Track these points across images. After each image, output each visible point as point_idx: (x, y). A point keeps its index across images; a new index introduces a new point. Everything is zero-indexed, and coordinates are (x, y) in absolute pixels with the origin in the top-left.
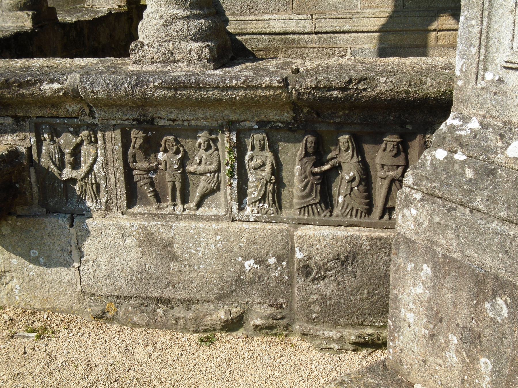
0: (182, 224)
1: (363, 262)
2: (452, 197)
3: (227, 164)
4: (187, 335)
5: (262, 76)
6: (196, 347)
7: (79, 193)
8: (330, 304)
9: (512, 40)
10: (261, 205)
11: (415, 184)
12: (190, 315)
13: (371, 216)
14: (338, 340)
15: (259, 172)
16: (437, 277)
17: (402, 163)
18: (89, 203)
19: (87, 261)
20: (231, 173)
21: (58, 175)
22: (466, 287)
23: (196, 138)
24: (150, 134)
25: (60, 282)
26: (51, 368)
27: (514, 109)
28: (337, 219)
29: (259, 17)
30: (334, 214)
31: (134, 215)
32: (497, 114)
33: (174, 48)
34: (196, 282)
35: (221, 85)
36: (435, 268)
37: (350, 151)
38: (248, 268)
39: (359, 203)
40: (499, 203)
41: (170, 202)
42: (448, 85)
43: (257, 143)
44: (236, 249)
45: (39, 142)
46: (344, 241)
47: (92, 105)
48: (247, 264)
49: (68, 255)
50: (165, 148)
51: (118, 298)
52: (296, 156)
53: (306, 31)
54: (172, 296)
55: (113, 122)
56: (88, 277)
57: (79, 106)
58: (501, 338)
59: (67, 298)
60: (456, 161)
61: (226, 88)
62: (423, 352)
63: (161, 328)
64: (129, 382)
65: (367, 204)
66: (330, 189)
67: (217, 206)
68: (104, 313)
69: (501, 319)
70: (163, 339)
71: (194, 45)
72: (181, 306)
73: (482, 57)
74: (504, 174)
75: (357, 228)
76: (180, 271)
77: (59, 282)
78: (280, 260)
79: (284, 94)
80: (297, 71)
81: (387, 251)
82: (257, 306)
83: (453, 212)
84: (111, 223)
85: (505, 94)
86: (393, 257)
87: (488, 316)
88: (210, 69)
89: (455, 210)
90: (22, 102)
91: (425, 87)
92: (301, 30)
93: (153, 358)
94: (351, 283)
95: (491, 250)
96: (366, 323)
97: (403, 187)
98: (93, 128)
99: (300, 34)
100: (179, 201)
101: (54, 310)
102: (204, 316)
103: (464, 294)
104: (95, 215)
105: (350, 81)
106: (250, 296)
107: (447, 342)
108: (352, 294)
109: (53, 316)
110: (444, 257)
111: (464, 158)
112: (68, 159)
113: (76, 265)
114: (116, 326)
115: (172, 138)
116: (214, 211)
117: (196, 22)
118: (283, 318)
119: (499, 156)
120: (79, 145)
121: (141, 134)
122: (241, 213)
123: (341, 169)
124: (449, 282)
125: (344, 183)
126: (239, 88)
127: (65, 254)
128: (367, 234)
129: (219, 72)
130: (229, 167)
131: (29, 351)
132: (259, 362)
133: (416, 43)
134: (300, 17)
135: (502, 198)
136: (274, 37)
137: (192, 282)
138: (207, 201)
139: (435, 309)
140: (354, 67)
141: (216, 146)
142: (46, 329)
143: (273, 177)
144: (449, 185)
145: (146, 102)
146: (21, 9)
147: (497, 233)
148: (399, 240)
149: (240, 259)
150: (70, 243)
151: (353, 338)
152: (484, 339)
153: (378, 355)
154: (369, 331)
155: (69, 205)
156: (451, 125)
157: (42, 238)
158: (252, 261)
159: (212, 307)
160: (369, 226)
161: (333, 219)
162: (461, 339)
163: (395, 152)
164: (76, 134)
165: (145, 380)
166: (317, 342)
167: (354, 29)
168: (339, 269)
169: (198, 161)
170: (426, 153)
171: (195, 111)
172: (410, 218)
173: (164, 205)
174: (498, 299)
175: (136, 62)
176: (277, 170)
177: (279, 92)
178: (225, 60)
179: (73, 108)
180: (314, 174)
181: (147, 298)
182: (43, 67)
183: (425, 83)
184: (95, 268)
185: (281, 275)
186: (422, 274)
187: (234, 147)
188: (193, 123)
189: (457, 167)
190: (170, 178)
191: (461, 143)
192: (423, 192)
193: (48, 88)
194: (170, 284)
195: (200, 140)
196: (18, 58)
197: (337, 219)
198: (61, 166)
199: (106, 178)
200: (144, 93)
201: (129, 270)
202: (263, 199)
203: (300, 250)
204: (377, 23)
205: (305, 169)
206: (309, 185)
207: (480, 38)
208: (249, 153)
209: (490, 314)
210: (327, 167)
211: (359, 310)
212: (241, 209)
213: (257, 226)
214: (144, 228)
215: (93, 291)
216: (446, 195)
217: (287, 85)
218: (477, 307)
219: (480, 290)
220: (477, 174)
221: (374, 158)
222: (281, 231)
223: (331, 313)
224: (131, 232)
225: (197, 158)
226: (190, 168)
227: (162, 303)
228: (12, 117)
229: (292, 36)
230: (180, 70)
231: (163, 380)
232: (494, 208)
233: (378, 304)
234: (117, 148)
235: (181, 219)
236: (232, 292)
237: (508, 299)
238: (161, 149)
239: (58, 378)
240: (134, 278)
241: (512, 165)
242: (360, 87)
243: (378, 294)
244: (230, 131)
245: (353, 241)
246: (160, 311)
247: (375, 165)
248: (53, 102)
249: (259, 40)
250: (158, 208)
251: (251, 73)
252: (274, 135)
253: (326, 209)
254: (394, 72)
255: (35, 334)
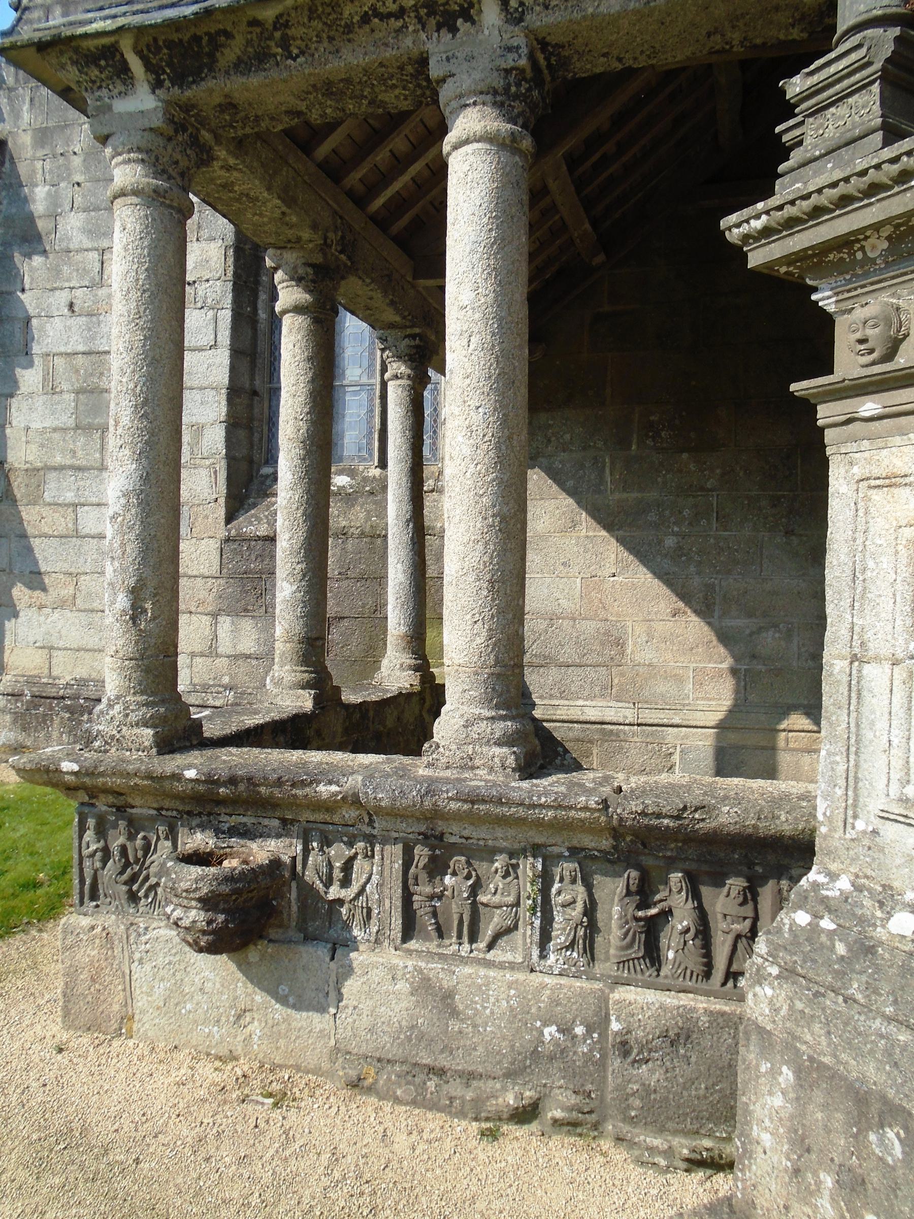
0: (468, 970)
1: (699, 1044)
2: (819, 979)
3: (528, 898)
4: (464, 1123)
5: (576, 794)
6: (475, 1143)
7: (345, 918)
8: (655, 1099)
9: (888, 785)
10: (569, 953)
11: (769, 954)
12: (469, 1096)
13: (710, 981)
14: (665, 1152)
15: (568, 910)
16: (801, 1086)
17: (751, 914)
18: (356, 932)
19: (346, 1007)
20: (533, 909)
21: (323, 894)
22: (842, 1107)
23: (493, 862)
24: (438, 852)
25: (310, 1032)
26: (287, 1153)
27: (895, 870)
28: (666, 981)
29: (571, 703)
30: (662, 974)
31: (410, 952)
32: (873, 874)
33: (474, 752)
34: (480, 1049)
35: (527, 802)
36: (798, 1072)
37: (684, 893)
38: (547, 1037)
39: (694, 962)
40: (882, 995)
41: (454, 940)
42: (807, 821)
43: (566, 873)
44: (533, 1010)
45: (306, 851)
46: (675, 1012)
47: (372, 813)
48: (547, 1031)
49: (324, 996)
50: (454, 871)
51: (379, 1060)
52: (615, 894)
53: (627, 722)
54: (447, 1065)
55: (396, 835)
56: (345, 1029)
57: (357, 813)
58: (894, 1188)
59: (316, 1054)
60: (823, 930)
61: (534, 806)
62: (785, 1193)
63: (430, 1109)
64: (383, 1186)
65: (705, 965)
66: (657, 939)
67: (513, 949)
68: (360, 1079)
69: (894, 1161)
70: (432, 1126)
71: (497, 750)
72: (458, 1080)
73: (850, 802)
74: (887, 956)
75: (691, 995)
76: (461, 1032)
77: (310, 1031)
78: (590, 1030)
79: (603, 818)
80: (620, 790)
81: (732, 1031)
82: (558, 1091)
83: (821, 999)
84: (381, 960)
85: (882, 850)
86: (742, 1050)
87: (874, 1153)
88: (515, 780)
89: (824, 996)
90: (294, 803)
91: (777, 822)
92: (621, 720)
93: (417, 1152)
94: (683, 1071)
95: (874, 1057)
96: (703, 1132)
97: (754, 956)
98: (370, 840)
99: (620, 724)
100: (465, 939)
101: (298, 1068)
102: (488, 1098)
103: (839, 1116)
104: (361, 948)
105: (685, 808)
106: (549, 1076)
107: (818, 1183)
108: (684, 1088)
109: (297, 1077)
110: (811, 1059)
111: (833, 926)
112: (337, 874)
113: (332, 1011)
114: (373, 1100)
115: (463, 859)
116: (509, 957)
117: (502, 724)
118: (591, 1112)
119: (879, 929)
120: (352, 859)
121: (426, 851)
122: (543, 962)
123: (672, 915)
124: (819, 1096)
125: (676, 934)
126: (549, 807)
127: (321, 995)
128: (705, 1005)
129: (525, 784)
130: (530, 902)
131: (262, 1125)
132: (557, 1174)
133: (761, 744)
134: (620, 704)
135: (885, 988)
136: (588, 726)
137: (475, 1049)
138: (502, 942)
139: (800, 1132)
140: (688, 788)
141: (516, 873)
142: (286, 1094)
143: (585, 919)
144: (814, 961)
145: (436, 814)
146: (303, 688)
147: (882, 1036)
148: (750, 1028)
149: (538, 1024)
150: (327, 982)
151: (685, 1151)
152: (870, 1186)
153: (722, 1184)
154: (707, 1143)
155: (332, 932)
156: (815, 881)
157: (295, 971)
158: (554, 1028)
159: (498, 1086)
160: (707, 994)
161: (660, 980)
162: (837, 1182)
163: (741, 899)
164: (350, 844)
165: (405, 1185)
166: (637, 1153)
167: (685, 723)
168: (668, 1050)
169: (493, 890)
170: (782, 914)
171: (493, 828)
172: (764, 999)
173: (447, 942)
174: (887, 1130)
175: (429, 765)
176: (590, 910)
177: (596, 815)
178: (533, 769)
179: (350, 814)
180: (637, 919)
181: (415, 1064)
182: (322, 763)
183: (778, 818)
184: (355, 1017)
185: (591, 1051)
186: (781, 1079)
187: (539, 876)
188: (490, 843)
189: (823, 938)
190: (457, 908)
191: (828, 906)
192: (780, 966)
193: (325, 790)
194: (447, 1049)
195: (496, 864)
196: (294, 748)
197: (666, 981)
198: (328, 883)
199: (380, 902)
200: (435, 804)
201: (397, 1025)
202: (571, 946)
203: (618, 1019)
204: (715, 717)
205: (626, 911)
206: (631, 933)
207: (847, 778)
208: (557, 886)
209: (877, 1151)
210: (653, 911)
211: (694, 1111)
212: (543, 956)
213: (562, 982)
214: (420, 971)
215: (350, 1048)
216: (811, 975)
217: (607, 807)
218: (859, 1138)
219: (861, 1114)
220: (850, 950)
221: (714, 905)
222: (592, 992)
223: (656, 1112)
224: (404, 974)
225: (491, 886)
226: (483, 898)
227: (434, 1074)
228: (279, 819)
229: (610, 727)
230: (479, 780)
231: (428, 1188)
232: (876, 1001)
233: (723, 1108)
234: (396, 866)
235: (466, 963)
236: (526, 1068)
237: (901, 1132)
238: (450, 871)
239: (294, 1169)
240: (402, 1036)
241: (897, 944)
242: (697, 816)
243: (720, 1091)
244: (534, 857)
245: (687, 1013)
246: (431, 1085)
247: (715, 913)
248: (328, 806)
249: (570, 729)
250: (439, 946)
251: (563, 789)
252: (589, 864)
253: (652, 966)
254: (738, 800)
255: (271, 1100)
